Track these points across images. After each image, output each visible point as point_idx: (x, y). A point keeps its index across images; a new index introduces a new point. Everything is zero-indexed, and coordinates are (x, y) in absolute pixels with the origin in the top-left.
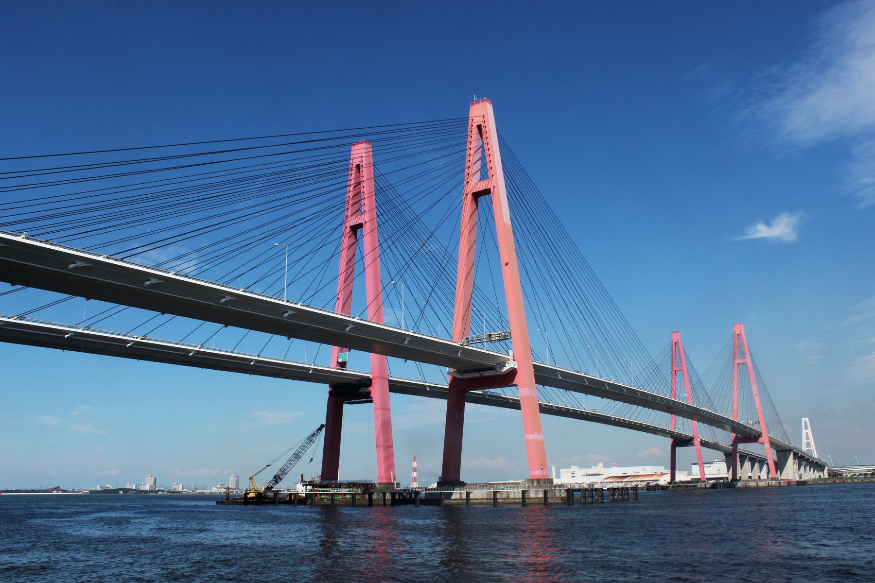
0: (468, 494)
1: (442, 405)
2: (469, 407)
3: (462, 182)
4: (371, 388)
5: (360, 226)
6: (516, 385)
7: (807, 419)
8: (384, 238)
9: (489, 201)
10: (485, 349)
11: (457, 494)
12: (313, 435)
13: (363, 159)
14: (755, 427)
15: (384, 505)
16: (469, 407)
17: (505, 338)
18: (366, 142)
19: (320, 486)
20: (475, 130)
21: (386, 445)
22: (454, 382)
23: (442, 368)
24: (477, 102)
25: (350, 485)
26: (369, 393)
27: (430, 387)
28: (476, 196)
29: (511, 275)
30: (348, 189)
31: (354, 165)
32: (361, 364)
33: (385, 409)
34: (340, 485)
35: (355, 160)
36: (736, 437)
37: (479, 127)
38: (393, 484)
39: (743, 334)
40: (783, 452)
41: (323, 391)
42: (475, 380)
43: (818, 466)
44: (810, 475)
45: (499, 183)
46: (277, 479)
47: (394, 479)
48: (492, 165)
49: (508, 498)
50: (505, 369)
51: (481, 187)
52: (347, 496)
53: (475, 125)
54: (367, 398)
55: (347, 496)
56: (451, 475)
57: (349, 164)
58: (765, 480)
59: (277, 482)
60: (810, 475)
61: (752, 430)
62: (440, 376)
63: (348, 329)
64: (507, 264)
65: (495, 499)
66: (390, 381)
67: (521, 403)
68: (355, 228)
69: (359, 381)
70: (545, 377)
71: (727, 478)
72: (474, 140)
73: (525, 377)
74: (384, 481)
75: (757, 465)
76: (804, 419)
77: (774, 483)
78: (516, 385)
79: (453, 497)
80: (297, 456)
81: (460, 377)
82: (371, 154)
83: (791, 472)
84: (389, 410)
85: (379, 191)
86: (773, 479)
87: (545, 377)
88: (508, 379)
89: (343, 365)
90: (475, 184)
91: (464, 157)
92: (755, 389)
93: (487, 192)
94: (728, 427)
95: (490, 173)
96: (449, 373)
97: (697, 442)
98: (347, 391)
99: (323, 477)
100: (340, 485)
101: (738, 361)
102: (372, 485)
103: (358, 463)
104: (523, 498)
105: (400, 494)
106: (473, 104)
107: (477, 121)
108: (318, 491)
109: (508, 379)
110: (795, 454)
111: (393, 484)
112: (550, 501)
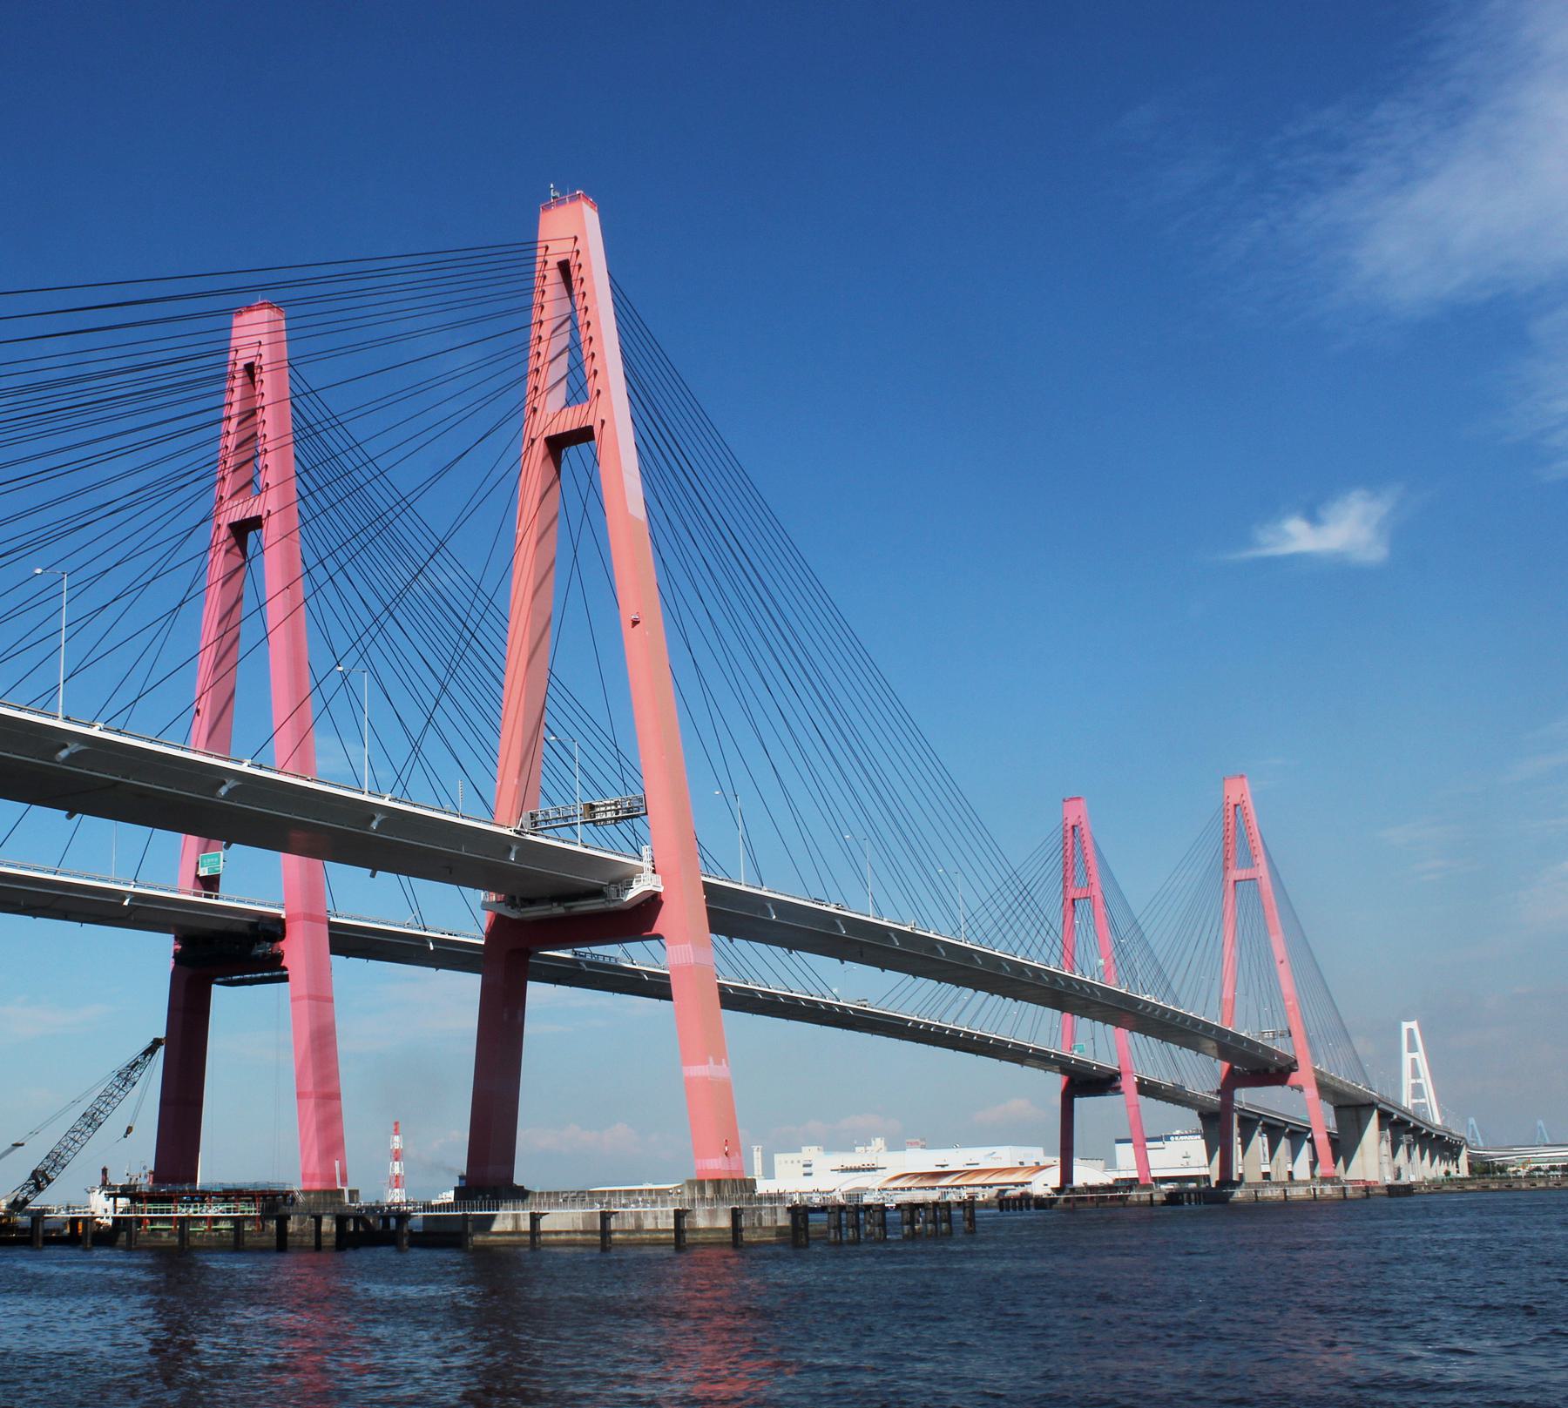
4: (283, 945)
5: (256, 523)
6: (659, 937)
7: (1414, 1025)
10: (579, 842)
11: (507, 1219)
12: (133, 1066)
13: (264, 350)
14: (1280, 1046)
15: (318, 1247)
17: (631, 813)
19: (151, 1198)
20: (553, 275)
22: (499, 928)
23: (467, 891)
24: (560, 202)
25: (229, 1195)
26: (279, 957)
27: (436, 941)
28: (557, 445)
29: (646, 651)
31: (240, 366)
33: (321, 999)
34: (203, 1197)
35: (242, 354)
36: (1231, 1071)
37: (564, 267)
39: (1250, 804)
40: (1352, 1111)
41: (160, 949)
42: (554, 923)
43: (1443, 1146)
44: (1422, 1169)
45: (614, 411)
46: (39, 1180)
47: (344, 1180)
49: (639, 1229)
50: (631, 895)
51: (569, 421)
52: (222, 1225)
53: (553, 262)
54: (271, 969)
55: (222, 1225)
56: (490, 1170)
58: (1304, 1183)
59: (39, 1188)
60: (1422, 1169)
61: (1272, 1052)
62: (463, 914)
63: (374, 825)
64: (635, 623)
65: (605, 1231)
66: (332, 925)
68: (243, 530)
69: (253, 926)
70: (733, 915)
71: (1207, 1178)
72: (551, 301)
73: (683, 916)
74: (317, 1185)
75: (1284, 1144)
76: (1405, 1026)
77: (1328, 1189)
78: (659, 937)
79: (496, 1227)
80: (92, 1120)
81: (513, 914)
83: (1374, 1161)
84: (331, 1000)
86: (1325, 1180)
87: (733, 915)
88: (640, 919)
90: (553, 414)
91: (526, 346)
92: (1279, 947)
94: (1210, 1045)
95: (592, 385)
97: (1128, 1083)
98: (222, 951)
99: (158, 1175)
100: (203, 1197)
101: (1235, 874)
103: (251, 1138)
104: (679, 1230)
105: (359, 1218)
106: (547, 207)
107: (558, 250)
108: (147, 1211)
109: (640, 919)
110: (1384, 1117)
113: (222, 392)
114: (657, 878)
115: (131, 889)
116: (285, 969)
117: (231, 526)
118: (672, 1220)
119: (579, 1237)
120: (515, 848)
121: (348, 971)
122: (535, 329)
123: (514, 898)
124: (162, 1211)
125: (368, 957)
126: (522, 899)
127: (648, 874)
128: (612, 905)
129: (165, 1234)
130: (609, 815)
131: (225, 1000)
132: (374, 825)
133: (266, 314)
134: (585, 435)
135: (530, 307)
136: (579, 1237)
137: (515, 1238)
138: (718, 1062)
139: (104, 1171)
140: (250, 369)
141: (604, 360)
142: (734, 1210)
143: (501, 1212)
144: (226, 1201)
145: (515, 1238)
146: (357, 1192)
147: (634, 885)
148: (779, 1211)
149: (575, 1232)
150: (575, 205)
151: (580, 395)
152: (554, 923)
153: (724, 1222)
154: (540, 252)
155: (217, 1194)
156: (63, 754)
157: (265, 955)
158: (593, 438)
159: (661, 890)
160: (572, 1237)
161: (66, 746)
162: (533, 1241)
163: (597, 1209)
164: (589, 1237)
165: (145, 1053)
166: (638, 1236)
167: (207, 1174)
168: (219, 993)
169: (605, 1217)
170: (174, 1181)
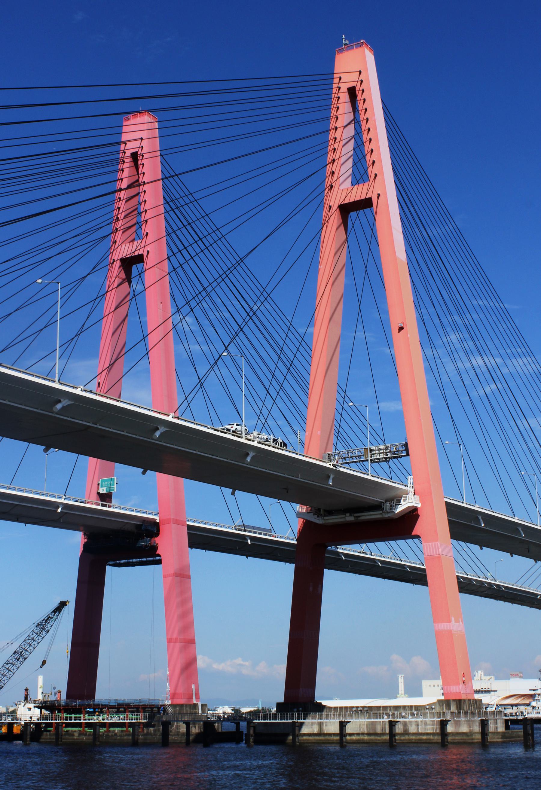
0: (343, 725)
1: (284, 573)
2: (332, 578)
3: (321, 190)
4: (157, 540)
5: (139, 259)
6: (418, 537)
8: (185, 297)
9: (370, 217)
11: (310, 726)
12: (47, 620)
13: (144, 143)
15: (188, 743)
16: (332, 578)
18: (149, 111)
19: (68, 709)
20: (345, 97)
21: (183, 640)
22: (308, 530)
23: (285, 504)
24: (349, 48)
25: (120, 707)
28: (346, 210)
29: (409, 348)
30: (117, 195)
31: (128, 153)
32: (137, 493)
33: (182, 576)
34: (100, 708)
35: (129, 145)
37: (352, 92)
38: (196, 706)
41: (72, 542)
42: (343, 524)
45: (385, 187)
48: (374, 157)
50: (400, 509)
51: (358, 193)
53: (344, 87)
54: (150, 556)
56: (300, 693)
57: (118, 152)
62: (283, 520)
63: (249, 459)
64: (401, 329)
66: (190, 527)
67: (427, 570)
68: (130, 263)
69: (138, 527)
70: (466, 526)
73: (434, 525)
74: (182, 701)
78: (418, 537)
80: (20, 656)
82: (157, 133)
84: (189, 577)
85: (171, 204)
87: (466, 526)
88: (404, 526)
89: (106, 498)
90: (343, 191)
93: (367, 203)
95: (372, 171)
96: (299, 515)
98: (118, 543)
100: (100, 708)
102: (162, 708)
103: (134, 668)
106: (341, 51)
107: (348, 80)
108: (63, 718)
109: (404, 526)
111: (196, 706)
112: (490, 738)
113: (117, 171)
114: (417, 498)
115: (62, 501)
116: (159, 555)
117: (123, 260)
118: (438, 727)
119: (366, 738)
120: (332, 476)
121: (202, 560)
122: (332, 133)
123: (319, 510)
124: (75, 719)
125: (206, 549)
126: (325, 511)
127: (411, 495)
128: (387, 516)
129: (76, 734)
130: (382, 456)
131: (114, 576)
132: (249, 459)
133: (146, 118)
134: (366, 204)
135: (328, 118)
136: (366, 738)
137: (322, 738)
138: (457, 621)
139: (27, 690)
140: (135, 156)
141: (379, 154)
142: (482, 720)
143: (306, 721)
144: (118, 712)
145: (322, 738)
146: (206, 705)
147: (402, 502)
148: (499, 721)
149: (363, 734)
150: (360, 50)
151: (365, 177)
152: (343, 524)
153: (477, 728)
154: (336, 81)
155: (112, 707)
156: (59, 406)
157: (146, 546)
158: (371, 205)
159: (419, 505)
160: (361, 737)
161: (60, 401)
162: (341, 739)
163: (386, 719)
164: (372, 737)
165: (54, 611)
166: (407, 737)
167: (102, 694)
168: (110, 571)
169: (392, 724)
170: (82, 697)
